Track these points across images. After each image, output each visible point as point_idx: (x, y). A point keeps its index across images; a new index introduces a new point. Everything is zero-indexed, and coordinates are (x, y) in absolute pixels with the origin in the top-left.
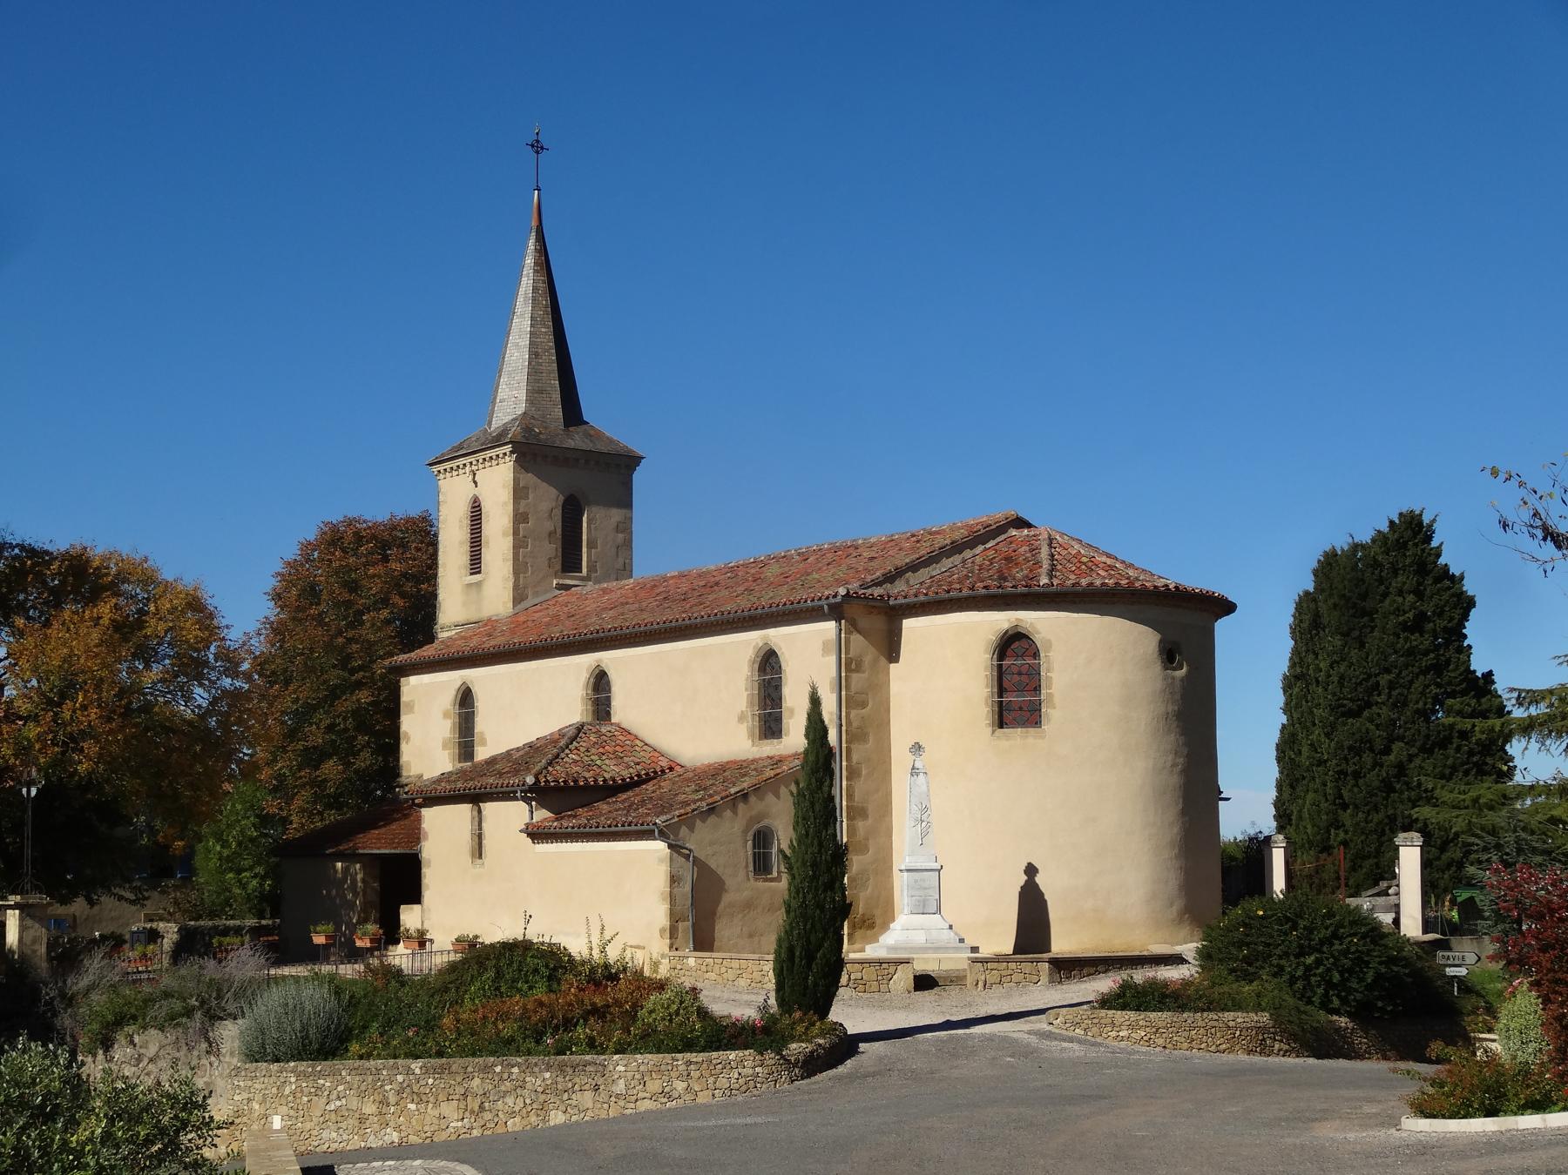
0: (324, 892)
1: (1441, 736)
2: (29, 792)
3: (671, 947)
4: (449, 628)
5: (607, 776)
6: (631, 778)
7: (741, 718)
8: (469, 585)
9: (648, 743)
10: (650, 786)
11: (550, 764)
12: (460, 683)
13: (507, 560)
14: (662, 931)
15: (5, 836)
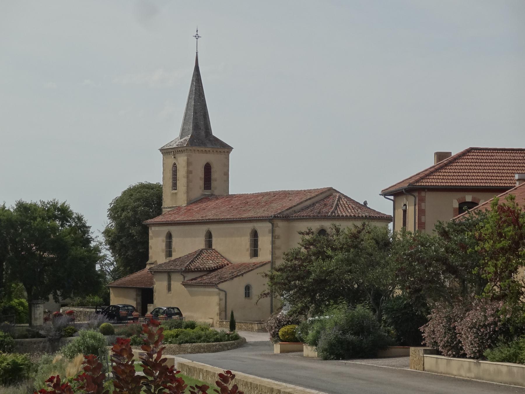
0: (341, 288)
1: (468, 253)
2: (37, 270)
3: (220, 318)
4: (166, 208)
5: (207, 267)
6: (215, 268)
7: (247, 250)
8: (173, 194)
9: (222, 255)
10: (219, 270)
11: (190, 263)
12: (168, 231)
13: (185, 187)
14: (217, 314)
15: (62, 290)
